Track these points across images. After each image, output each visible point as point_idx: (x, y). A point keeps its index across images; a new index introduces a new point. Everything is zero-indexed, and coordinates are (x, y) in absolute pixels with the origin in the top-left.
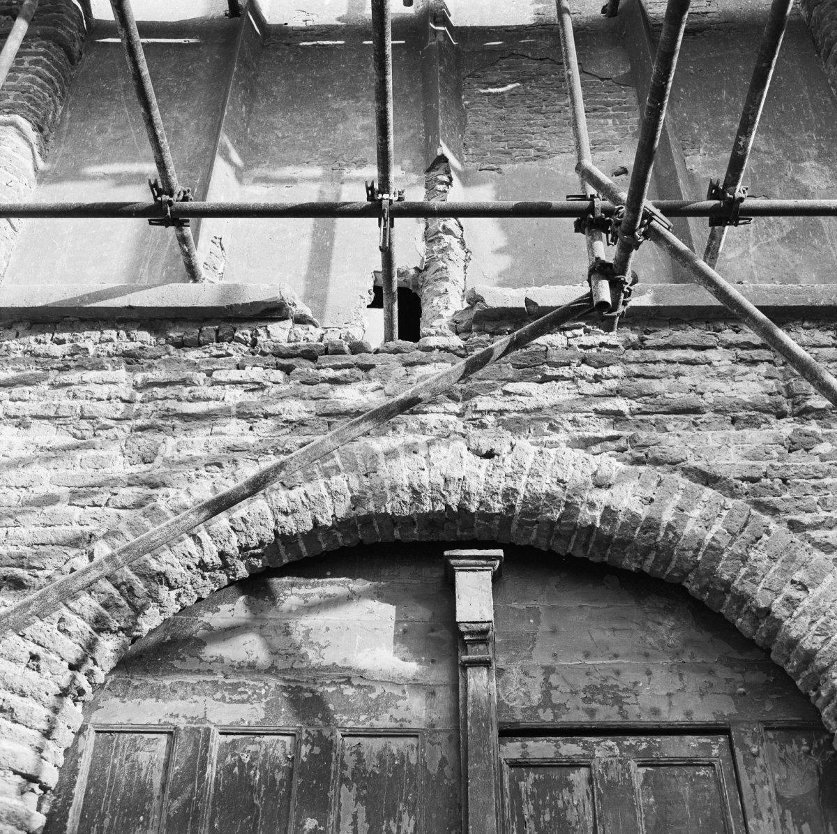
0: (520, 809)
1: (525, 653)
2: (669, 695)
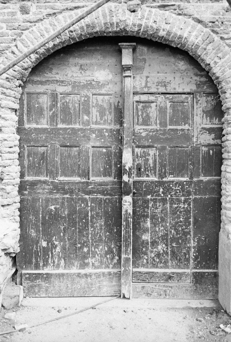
0: (138, 113)
1: (141, 72)
2: (179, 84)
